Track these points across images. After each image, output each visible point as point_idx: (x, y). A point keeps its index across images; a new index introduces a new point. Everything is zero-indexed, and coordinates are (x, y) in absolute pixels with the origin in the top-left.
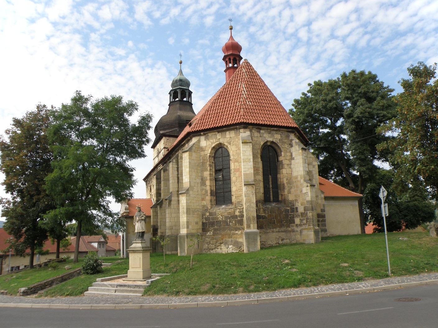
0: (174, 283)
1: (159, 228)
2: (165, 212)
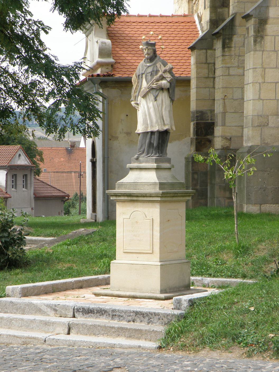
0: (268, 313)
1: (219, 120)
2: (241, 65)
